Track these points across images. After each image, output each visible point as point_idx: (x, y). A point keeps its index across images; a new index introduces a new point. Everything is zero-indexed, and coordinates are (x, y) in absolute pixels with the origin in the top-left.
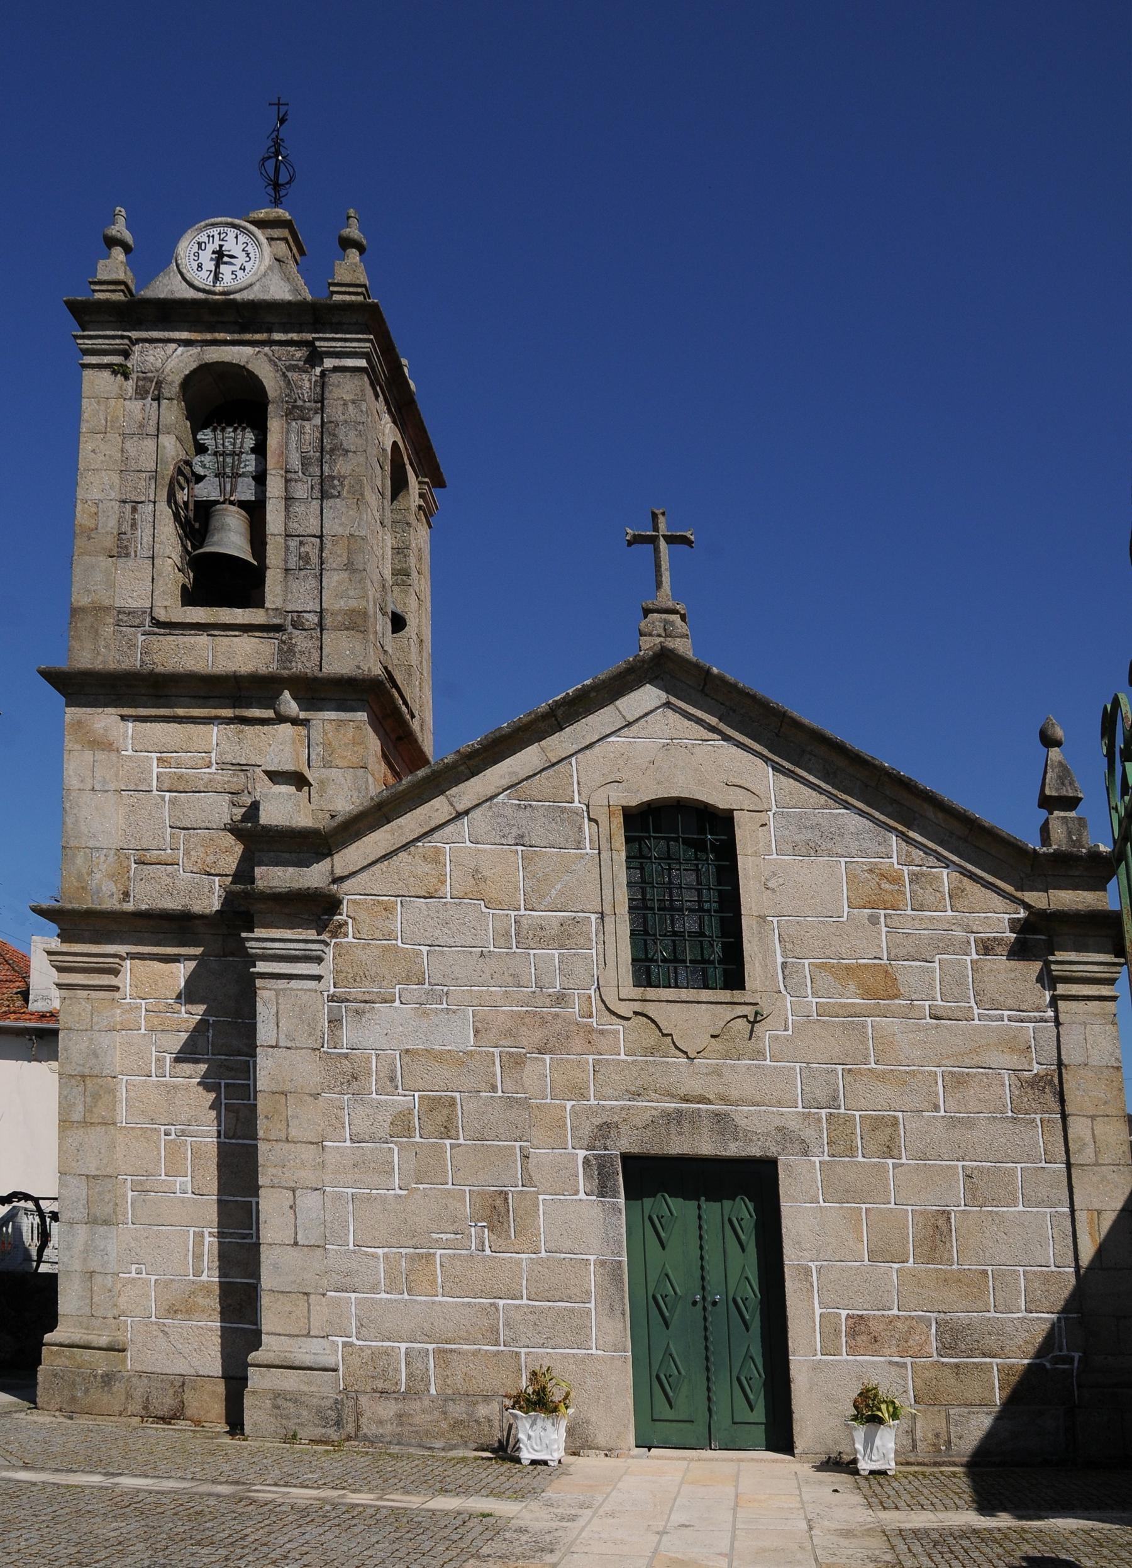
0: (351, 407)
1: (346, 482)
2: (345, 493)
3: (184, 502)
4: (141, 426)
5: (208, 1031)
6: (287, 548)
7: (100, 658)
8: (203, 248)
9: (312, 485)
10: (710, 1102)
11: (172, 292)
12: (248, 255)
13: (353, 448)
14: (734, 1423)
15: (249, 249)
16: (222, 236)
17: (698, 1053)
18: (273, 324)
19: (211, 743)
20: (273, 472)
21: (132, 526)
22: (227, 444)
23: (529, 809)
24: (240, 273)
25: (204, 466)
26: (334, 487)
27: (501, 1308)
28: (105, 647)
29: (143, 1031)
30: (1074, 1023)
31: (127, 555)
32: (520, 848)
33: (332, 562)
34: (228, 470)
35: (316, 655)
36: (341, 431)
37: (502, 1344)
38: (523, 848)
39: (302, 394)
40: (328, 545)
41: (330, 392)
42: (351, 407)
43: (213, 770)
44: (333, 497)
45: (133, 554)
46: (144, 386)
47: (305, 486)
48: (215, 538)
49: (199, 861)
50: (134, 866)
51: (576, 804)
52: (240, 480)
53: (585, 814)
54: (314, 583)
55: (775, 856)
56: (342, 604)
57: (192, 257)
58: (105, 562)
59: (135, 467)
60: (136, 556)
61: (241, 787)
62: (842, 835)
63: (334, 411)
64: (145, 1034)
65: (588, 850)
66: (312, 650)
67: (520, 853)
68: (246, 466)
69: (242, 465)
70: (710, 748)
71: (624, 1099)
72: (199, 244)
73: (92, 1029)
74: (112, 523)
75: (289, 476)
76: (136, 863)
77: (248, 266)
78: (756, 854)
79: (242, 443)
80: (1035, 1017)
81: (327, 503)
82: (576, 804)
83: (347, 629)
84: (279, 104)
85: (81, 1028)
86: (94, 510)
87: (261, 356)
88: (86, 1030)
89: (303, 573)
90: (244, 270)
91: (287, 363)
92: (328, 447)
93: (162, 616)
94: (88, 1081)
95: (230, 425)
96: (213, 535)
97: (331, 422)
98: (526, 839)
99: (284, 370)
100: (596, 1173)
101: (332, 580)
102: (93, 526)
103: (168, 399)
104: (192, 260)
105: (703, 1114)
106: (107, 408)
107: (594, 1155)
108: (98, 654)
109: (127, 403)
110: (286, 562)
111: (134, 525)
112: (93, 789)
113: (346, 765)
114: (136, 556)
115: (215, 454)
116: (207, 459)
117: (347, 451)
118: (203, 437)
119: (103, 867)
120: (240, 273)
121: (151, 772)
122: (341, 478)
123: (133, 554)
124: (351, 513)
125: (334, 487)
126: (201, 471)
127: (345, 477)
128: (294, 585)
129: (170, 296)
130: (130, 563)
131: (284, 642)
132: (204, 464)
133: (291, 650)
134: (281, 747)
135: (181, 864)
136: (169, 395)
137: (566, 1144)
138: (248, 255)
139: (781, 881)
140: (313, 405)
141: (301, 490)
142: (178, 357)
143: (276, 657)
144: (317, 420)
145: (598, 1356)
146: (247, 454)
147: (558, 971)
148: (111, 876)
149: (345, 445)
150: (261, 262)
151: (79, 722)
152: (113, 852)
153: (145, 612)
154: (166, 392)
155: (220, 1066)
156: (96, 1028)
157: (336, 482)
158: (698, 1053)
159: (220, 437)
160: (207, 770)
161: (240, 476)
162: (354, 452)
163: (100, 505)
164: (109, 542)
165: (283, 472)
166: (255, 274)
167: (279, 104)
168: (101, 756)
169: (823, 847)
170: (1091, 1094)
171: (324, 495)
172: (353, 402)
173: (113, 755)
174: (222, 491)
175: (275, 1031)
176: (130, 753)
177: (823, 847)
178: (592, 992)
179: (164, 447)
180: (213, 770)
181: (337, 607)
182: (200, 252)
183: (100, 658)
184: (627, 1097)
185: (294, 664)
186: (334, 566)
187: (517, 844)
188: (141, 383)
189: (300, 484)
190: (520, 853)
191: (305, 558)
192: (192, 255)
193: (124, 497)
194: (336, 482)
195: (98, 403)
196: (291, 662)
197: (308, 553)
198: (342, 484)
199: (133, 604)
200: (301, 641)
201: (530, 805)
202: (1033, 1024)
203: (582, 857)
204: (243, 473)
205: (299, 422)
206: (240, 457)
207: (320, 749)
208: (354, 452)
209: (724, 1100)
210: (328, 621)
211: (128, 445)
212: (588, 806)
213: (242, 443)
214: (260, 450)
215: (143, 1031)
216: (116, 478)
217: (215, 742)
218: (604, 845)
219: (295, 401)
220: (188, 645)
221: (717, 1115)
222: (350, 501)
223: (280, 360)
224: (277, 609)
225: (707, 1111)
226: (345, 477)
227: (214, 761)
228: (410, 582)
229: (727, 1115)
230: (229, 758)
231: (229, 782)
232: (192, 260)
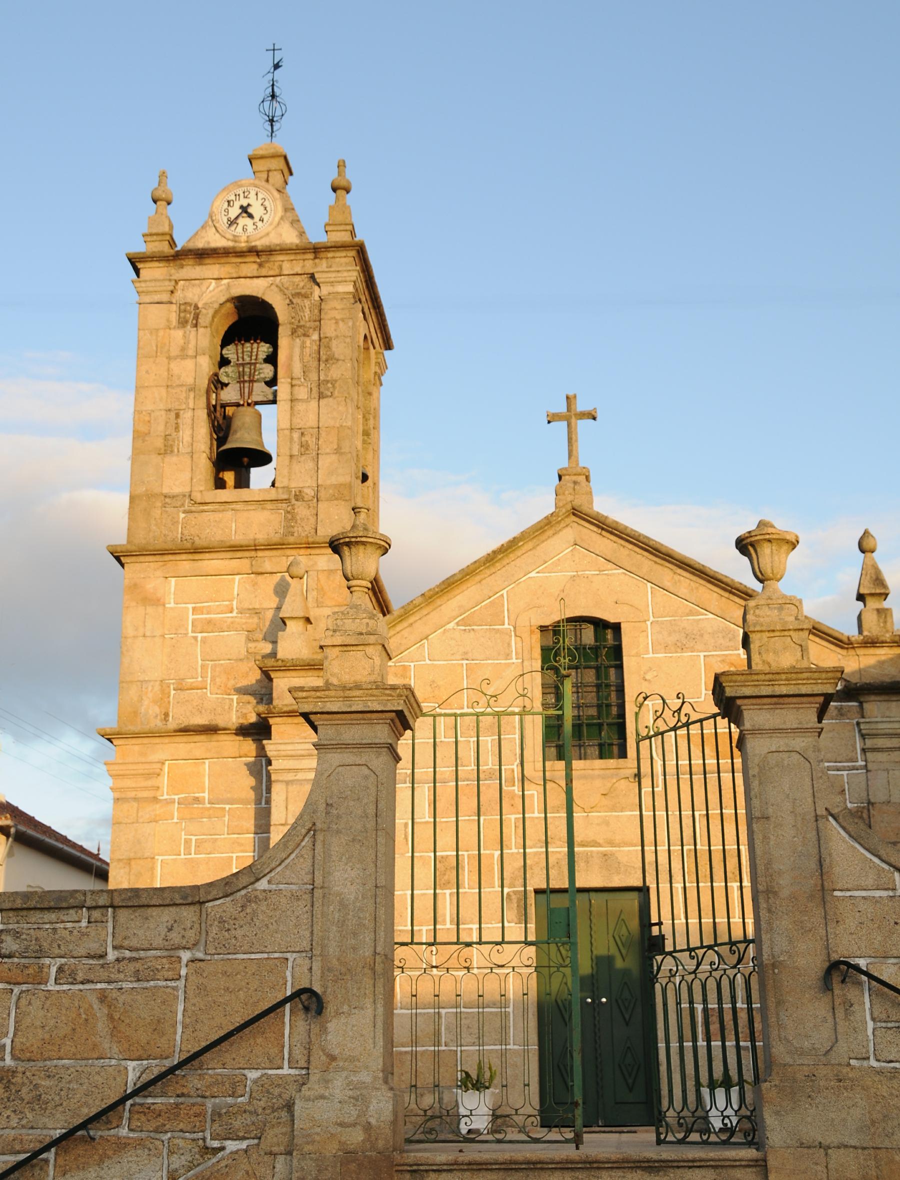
0: (341, 324)
1: (337, 385)
2: (336, 393)
3: (213, 406)
4: (183, 349)
5: (224, 816)
6: (291, 439)
7: (151, 534)
8: (232, 205)
9: (311, 389)
10: (600, 846)
11: (209, 243)
12: (265, 209)
13: (342, 357)
14: (616, 1103)
15: (267, 203)
16: (246, 194)
17: (592, 808)
18: (283, 261)
19: (233, 594)
20: (283, 380)
21: (176, 428)
22: (245, 357)
23: (472, 632)
24: (260, 224)
25: (228, 376)
26: (328, 389)
27: (443, 1015)
28: (156, 525)
29: (175, 820)
30: (880, 769)
31: (172, 451)
32: (465, 662)
33: (326, 448)
34: (246, 378)
35: (312, 520)
36: (334, 343)
37: (443, 1044)
38: (467, 662)
39: (305, 316)
40: (323, 434)
41: (326, 313)
42: (341, 324)
43: (234, 614)
44: (327, 397)
45: (176, 450)
46: (184, 318)
47: (306, 390)
48: (238, 435)
49: (222, 685)
50: (173, 692)
51: (506, 626)
52: (255, 384)
53: (513, 633)
54: (311, 465)
55: (651, 655)
56: (333, 480)
57: (223, 213)
58: (155, 459)
59: (178, 382)
60: (178, 451)
61: (255, 626)
62: (702, 635)
63: (329, 329)
64: (177, 823)
65: (514, 660)
66: (310, 517)
67: (465, 666)
68: (259, 373)
69: (257, 373)
70: (604, 577)
71: (537, 847)
72: (229, 202)
73: (137, 822)
74: (161, 428)
75: (294, 382)
76: (174, 690)
77: (266, 218)
78: (638, 655)
79: (257, 355)
80: (848, 766)
81: (323, 402)
82: (506, 626)
83: (337, 499)
84: (274, 50)
85: (129, 821)
86: (147, 418)
87: (273, 287)
88: (133, 823)
89: (304, 458)
90: (263, 221)
91: (293, 292)
92: (323, 358)
93: (198, 497)
94: (133, 863)
95: (247, 341)
96: (236, 432)
97: (326, 337)
98: (470, 654)
99: (291, 298)
100: (516, 905)
101: (324, 462)
102: (147, 431)
103: (204, 327)
104: (223, 216)
105: (594, 855)
106: (157, 336)
107: (514, 892)
108: (150, 531)
109: (172, 332)
110: (290, 449)
111: (177, 428)
112: (144, 636)
113: (334, 603)
114: (178, 451)
115: (238, 365)
116: (229, 369)
117: (338, 360)
118: (227, 352)
119: (150, 695)
120: (260, 224)
121: (188, 618)
122: (334, 382)
123: (176, 450)
124: (340, 408)
125: (328, 389)
126: (225, 379)
127: (336, 381)
128: (296, 467)
129: (206, 246)
130: (174, 459)
131: (288, 512)
132: (227, 374)
133: (293, 518)
134: (293, 598)
135: (208, 688)
136: (204, 325)
137: (494, 884)
138: (265, 209)
139: (655, 673)
140: (312, 324)
141: (302, 393)
142: (210, 292)
143: (283, 524)
144: (315, 337)
145: (515, 1050)
146: (261, 363)
147: (490, 753)
148: (155, 702)
149: (336, 356)
150: (275, 213)
151: (135, 585)
152: (158, 683)
153: (185, 496)
154: (201, 321)
155: (233, 843)
156: (141, 820)
157: (329, 385)
158: (592, 808)
159: (240, 351)
160: (230, 615)
161: (255, 381)
162: (344, 361)
163: (153, 415)
164: (159, 443)
165: (289, 380)
166: (271, 224)
167: (274, 50)
168: (150, 610)
169: (687, 646)
170: (892, 825)
171: (321, 396)
172: (343, 320)
173: (160, 609)
174: (242, 395)
175: (285, 813)
176: (172, 605)
177: (687, 646)
178: (515, 767)
179: (201, 365)
180: (234, 614)
181: (328, 482)
182: (229, 208)
183: (151, 534)
184: (539, 845)
185: (296, 529)
186: (328, 450)
187: (463, 659)
188: (182, 315)
189: (302, 388)
190: (465, 666)
191: (304, 446)
192: (223, 212)
193: (170, 407)
194: (329, 385)
195: (151, 333)
196: (293, 527)
197: (307, 441)
198: (334, 386)
199: (177, 490)
200: (302, 510)
201: (473, 630)
202: (847, 772)
203: (509, 665)
204: (258, 379)
205: (302, 338)
206: (255, 367)
207: (315, 593)
208: (344, 361)
209: (611, 843)
210: (322, 494)
211: (172, 365)
212: (515, 628)
213: (257, 355)
214: (272, 359)
215: (175, 820)
216: (163, 391)
217: (236, 593)
218: (526, 656)
219: (299, 322)
220: (217, 519)
221: (605, 855)
222: (340, 399)
223: (287, 289)
224: (284, 487)
225: (598, 852)
226: (336, 381)
227: (235, 607)
228: (369, 441)
229: (612, 854)
230: (246, 605)
231: (246, 623)
232: (223, 216)
